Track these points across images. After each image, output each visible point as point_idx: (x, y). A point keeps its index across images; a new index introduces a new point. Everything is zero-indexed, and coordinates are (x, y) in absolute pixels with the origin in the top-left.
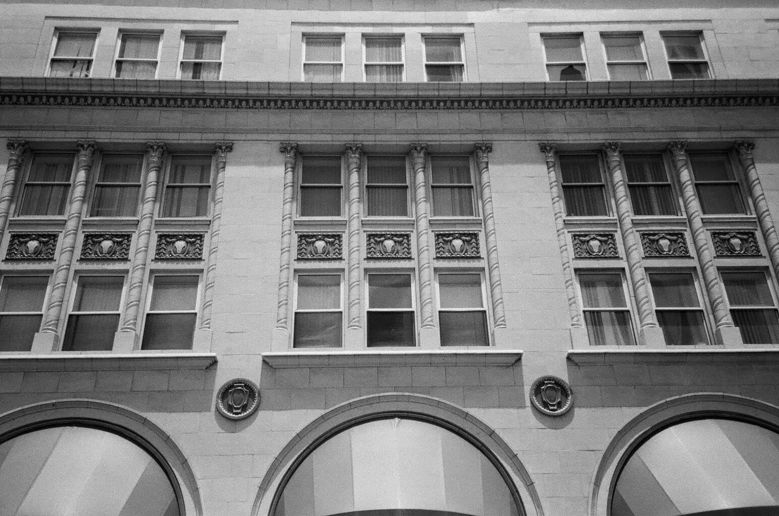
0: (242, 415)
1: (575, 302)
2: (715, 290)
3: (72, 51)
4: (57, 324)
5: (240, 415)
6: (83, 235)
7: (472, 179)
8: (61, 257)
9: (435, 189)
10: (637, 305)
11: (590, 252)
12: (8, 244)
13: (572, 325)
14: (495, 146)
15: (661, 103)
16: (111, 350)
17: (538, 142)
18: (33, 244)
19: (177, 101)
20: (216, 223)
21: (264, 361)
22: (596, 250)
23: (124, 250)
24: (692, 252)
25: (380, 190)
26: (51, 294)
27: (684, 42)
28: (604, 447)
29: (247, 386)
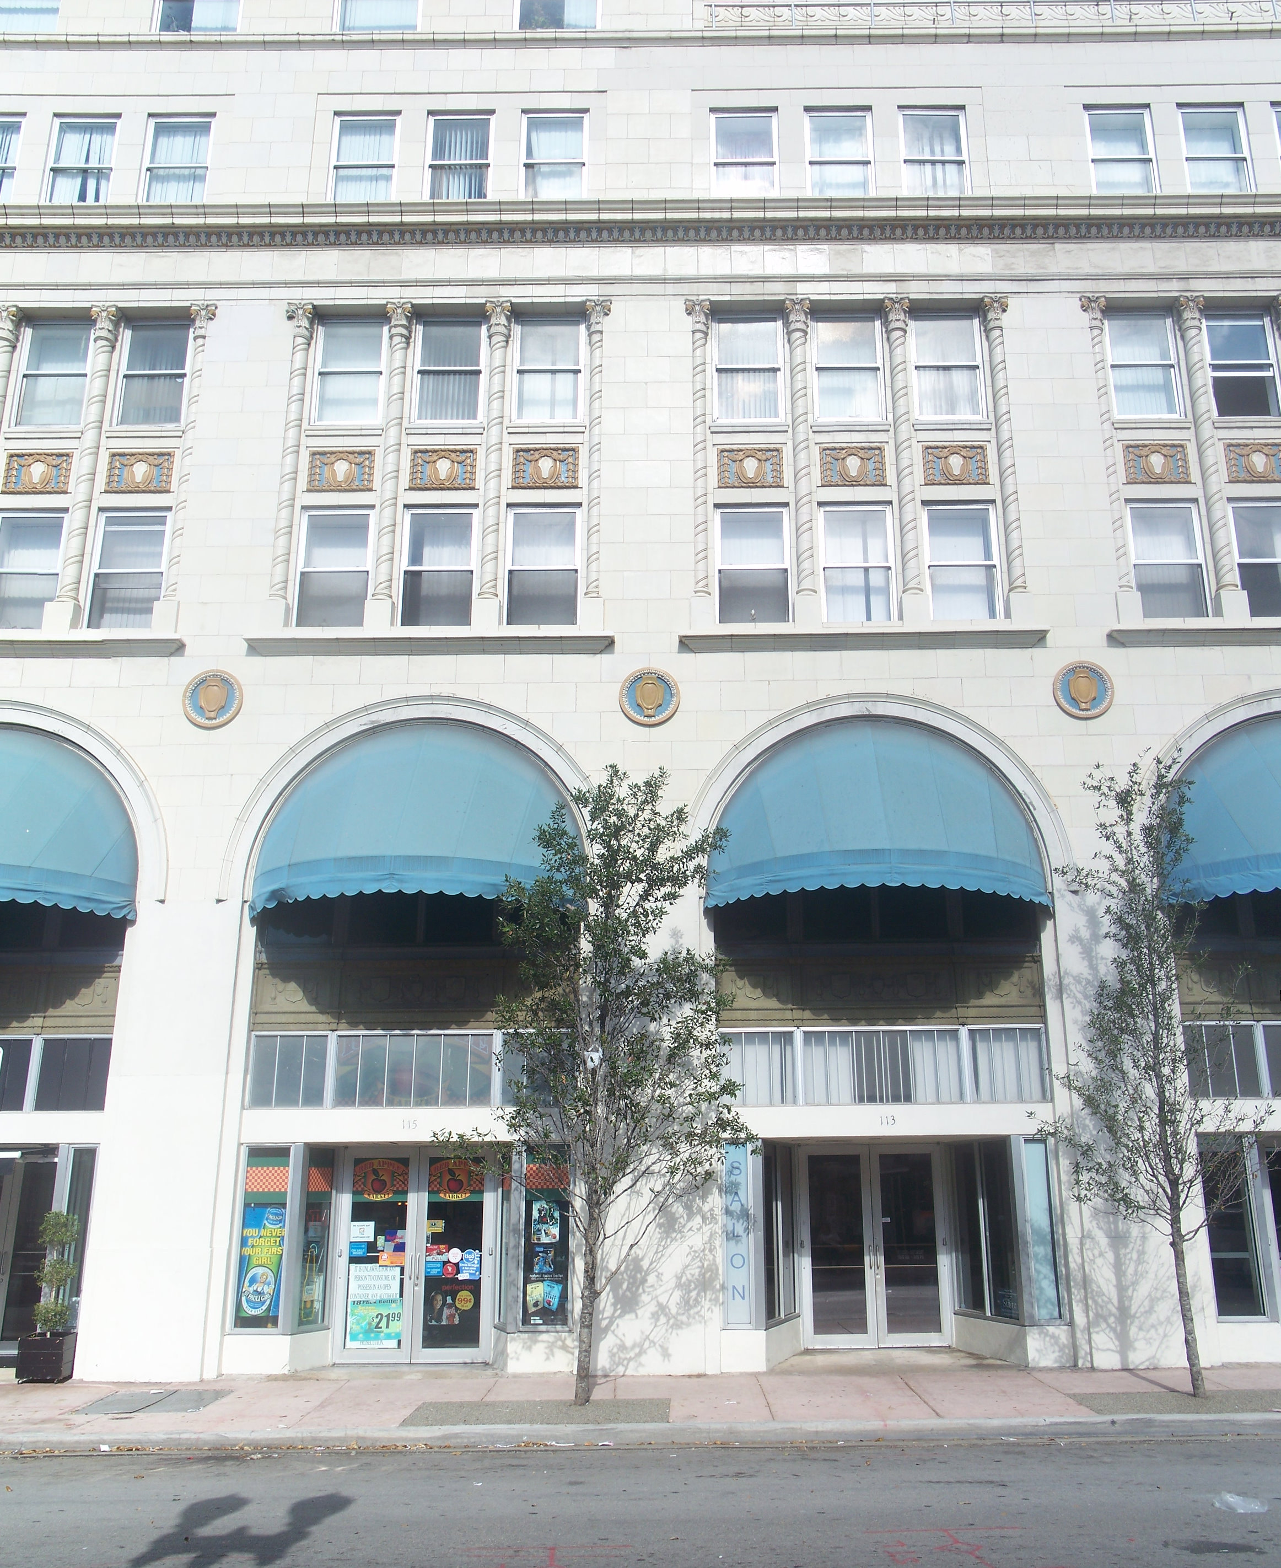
0: (218, 720)
1: (1125, 554)
2: (1221, 534)
3: (177, 150)
4: (286, 588)
5: (214, 721)
6: (107, 454)
7: (879, 354)
8: (78, 490)
9: (724, 375)
10: (1214, 557)
11: (1250, 470)
12: (106, 467)
13: (1120, 587)
14: (1012, 302)
15: (1074, 231)
16: (40, 627)
17: (1079, 295)
18: (38, 471)
19: (199, 236)
20: (190, 435)
21: (681, 642)
22: (956, 472)
23: (468, 475)
24: (1195, 475)
25: (740, 375)
26: (69, 542)
27: (461, 132)
28: (711, 766)
29: (660, 678)
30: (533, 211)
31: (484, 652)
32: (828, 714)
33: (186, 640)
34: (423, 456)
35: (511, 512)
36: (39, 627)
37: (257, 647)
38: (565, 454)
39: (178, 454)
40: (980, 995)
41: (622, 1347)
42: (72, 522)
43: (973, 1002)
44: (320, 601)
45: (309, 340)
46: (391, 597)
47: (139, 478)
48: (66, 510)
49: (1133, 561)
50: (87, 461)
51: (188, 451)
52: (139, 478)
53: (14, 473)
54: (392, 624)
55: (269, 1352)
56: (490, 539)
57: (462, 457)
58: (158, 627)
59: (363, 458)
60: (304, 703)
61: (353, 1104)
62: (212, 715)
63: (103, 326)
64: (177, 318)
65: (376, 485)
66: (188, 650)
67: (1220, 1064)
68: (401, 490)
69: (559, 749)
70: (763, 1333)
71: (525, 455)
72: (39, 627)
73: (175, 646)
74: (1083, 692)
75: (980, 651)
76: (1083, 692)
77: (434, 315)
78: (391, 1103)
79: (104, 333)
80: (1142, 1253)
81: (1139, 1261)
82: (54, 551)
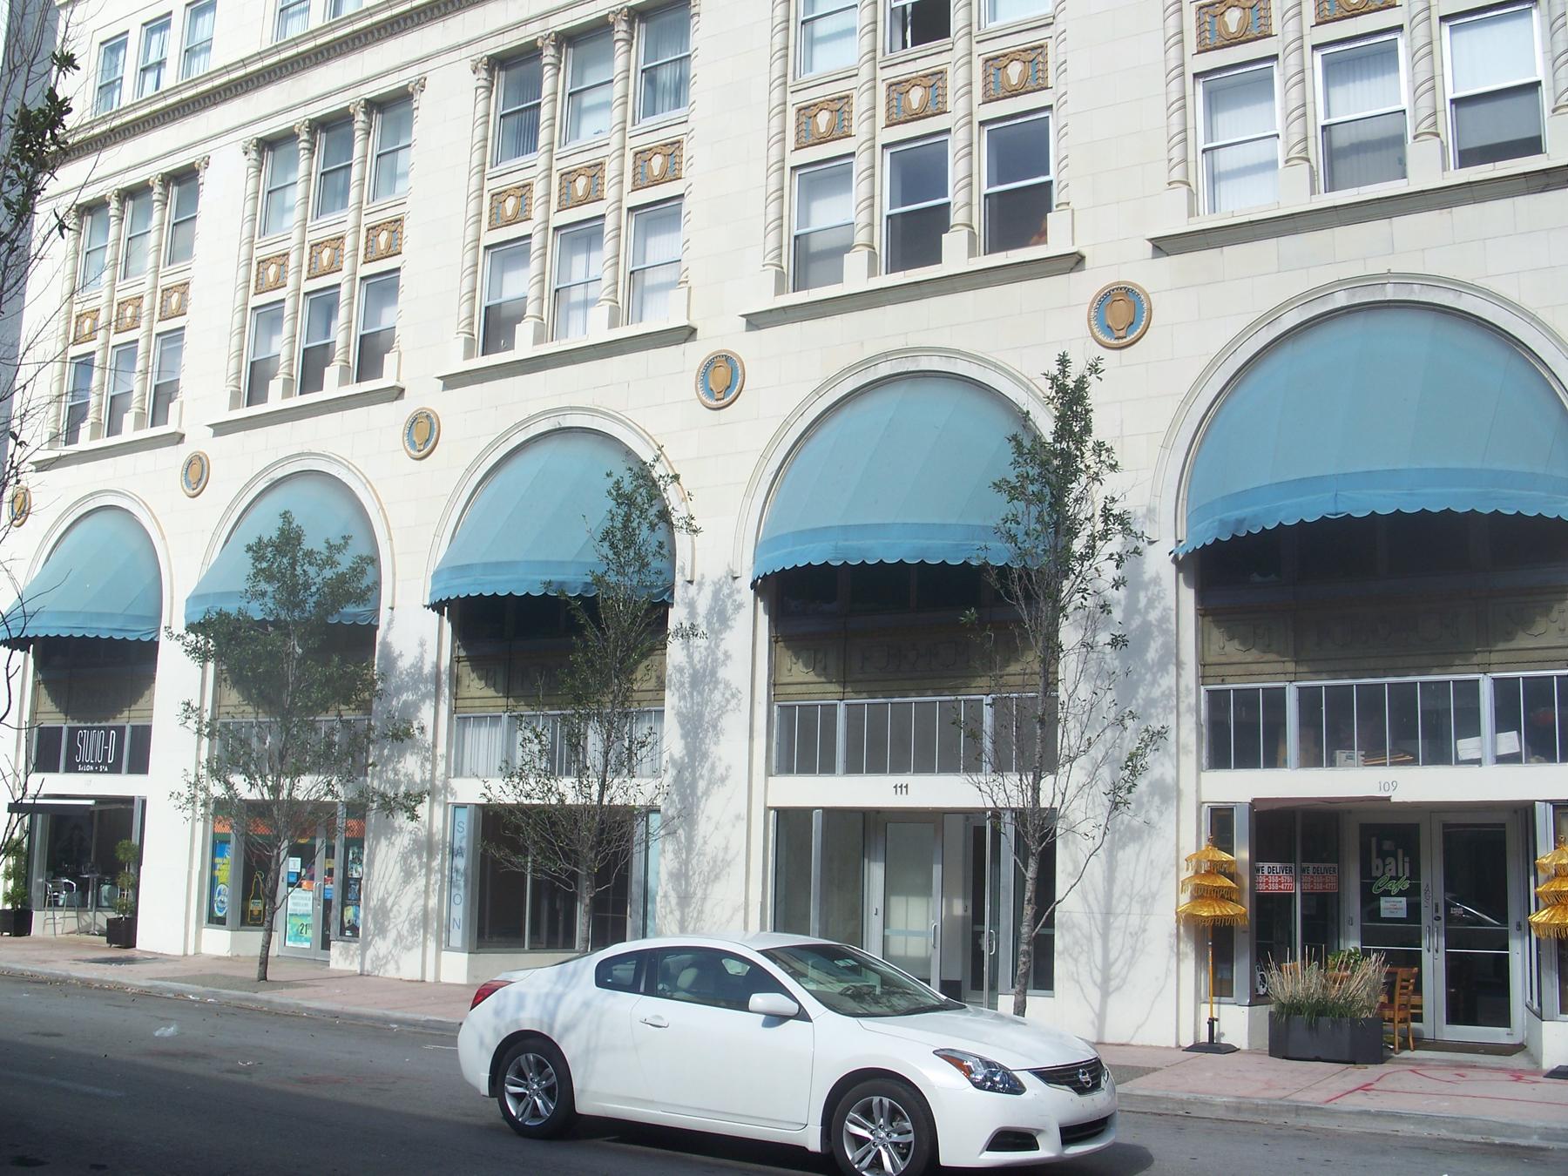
18: (916, 97)
26: (860, 189)
30: (371, 15)
31: (1295, 231)
32: (884, 370)
33: (1084, 252)
34: (898, 88)
35: (1318, 55)
36: (937, 259)
37: (755, 321)
38: (1034, 56)
39: (1051, 44)
40: (1509, 636)
41: (377, 957)
42: (860, 165)
43: (1501, 646)
44: (808, 259)
45: (489, 89)
46: (1308, 160)
47: (1233, 28)
48: (948, 131)
49: (1450, 95)
50: (962, 72)
51: (1061, 36)
52: (1233, 28)
53: (1207, 26)
54: (1444, 169)
55: (218, 942)
56: (1423, 65)
57: (933, 80)
58: (1057, 243)
59: (840, 105)
60: (796, 371)
61: (1321, 765)
62: (1121, 333)
63: (621, 29)
64: (528, 53)
65: (1276, 28)
66: (1088, 263)
67: (1247, 730)
68: (1307, 29)
69: (1533, 319)
70: (464, 957)
71: (995, 64)
72: (937, 259)
73: (1074, 260)
74: (722, 381)
75: (1508, 202)
76: (722, 381)
77: (513, 57)
78: (1239, 765)
79: (551, 60)
80: (701, 912)
81: (698, 919)
82: (1265, 106)
